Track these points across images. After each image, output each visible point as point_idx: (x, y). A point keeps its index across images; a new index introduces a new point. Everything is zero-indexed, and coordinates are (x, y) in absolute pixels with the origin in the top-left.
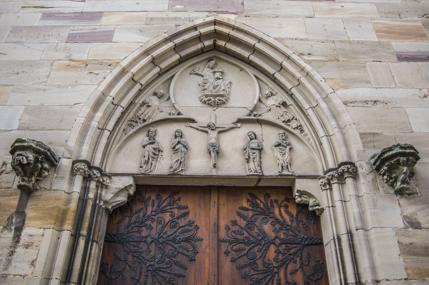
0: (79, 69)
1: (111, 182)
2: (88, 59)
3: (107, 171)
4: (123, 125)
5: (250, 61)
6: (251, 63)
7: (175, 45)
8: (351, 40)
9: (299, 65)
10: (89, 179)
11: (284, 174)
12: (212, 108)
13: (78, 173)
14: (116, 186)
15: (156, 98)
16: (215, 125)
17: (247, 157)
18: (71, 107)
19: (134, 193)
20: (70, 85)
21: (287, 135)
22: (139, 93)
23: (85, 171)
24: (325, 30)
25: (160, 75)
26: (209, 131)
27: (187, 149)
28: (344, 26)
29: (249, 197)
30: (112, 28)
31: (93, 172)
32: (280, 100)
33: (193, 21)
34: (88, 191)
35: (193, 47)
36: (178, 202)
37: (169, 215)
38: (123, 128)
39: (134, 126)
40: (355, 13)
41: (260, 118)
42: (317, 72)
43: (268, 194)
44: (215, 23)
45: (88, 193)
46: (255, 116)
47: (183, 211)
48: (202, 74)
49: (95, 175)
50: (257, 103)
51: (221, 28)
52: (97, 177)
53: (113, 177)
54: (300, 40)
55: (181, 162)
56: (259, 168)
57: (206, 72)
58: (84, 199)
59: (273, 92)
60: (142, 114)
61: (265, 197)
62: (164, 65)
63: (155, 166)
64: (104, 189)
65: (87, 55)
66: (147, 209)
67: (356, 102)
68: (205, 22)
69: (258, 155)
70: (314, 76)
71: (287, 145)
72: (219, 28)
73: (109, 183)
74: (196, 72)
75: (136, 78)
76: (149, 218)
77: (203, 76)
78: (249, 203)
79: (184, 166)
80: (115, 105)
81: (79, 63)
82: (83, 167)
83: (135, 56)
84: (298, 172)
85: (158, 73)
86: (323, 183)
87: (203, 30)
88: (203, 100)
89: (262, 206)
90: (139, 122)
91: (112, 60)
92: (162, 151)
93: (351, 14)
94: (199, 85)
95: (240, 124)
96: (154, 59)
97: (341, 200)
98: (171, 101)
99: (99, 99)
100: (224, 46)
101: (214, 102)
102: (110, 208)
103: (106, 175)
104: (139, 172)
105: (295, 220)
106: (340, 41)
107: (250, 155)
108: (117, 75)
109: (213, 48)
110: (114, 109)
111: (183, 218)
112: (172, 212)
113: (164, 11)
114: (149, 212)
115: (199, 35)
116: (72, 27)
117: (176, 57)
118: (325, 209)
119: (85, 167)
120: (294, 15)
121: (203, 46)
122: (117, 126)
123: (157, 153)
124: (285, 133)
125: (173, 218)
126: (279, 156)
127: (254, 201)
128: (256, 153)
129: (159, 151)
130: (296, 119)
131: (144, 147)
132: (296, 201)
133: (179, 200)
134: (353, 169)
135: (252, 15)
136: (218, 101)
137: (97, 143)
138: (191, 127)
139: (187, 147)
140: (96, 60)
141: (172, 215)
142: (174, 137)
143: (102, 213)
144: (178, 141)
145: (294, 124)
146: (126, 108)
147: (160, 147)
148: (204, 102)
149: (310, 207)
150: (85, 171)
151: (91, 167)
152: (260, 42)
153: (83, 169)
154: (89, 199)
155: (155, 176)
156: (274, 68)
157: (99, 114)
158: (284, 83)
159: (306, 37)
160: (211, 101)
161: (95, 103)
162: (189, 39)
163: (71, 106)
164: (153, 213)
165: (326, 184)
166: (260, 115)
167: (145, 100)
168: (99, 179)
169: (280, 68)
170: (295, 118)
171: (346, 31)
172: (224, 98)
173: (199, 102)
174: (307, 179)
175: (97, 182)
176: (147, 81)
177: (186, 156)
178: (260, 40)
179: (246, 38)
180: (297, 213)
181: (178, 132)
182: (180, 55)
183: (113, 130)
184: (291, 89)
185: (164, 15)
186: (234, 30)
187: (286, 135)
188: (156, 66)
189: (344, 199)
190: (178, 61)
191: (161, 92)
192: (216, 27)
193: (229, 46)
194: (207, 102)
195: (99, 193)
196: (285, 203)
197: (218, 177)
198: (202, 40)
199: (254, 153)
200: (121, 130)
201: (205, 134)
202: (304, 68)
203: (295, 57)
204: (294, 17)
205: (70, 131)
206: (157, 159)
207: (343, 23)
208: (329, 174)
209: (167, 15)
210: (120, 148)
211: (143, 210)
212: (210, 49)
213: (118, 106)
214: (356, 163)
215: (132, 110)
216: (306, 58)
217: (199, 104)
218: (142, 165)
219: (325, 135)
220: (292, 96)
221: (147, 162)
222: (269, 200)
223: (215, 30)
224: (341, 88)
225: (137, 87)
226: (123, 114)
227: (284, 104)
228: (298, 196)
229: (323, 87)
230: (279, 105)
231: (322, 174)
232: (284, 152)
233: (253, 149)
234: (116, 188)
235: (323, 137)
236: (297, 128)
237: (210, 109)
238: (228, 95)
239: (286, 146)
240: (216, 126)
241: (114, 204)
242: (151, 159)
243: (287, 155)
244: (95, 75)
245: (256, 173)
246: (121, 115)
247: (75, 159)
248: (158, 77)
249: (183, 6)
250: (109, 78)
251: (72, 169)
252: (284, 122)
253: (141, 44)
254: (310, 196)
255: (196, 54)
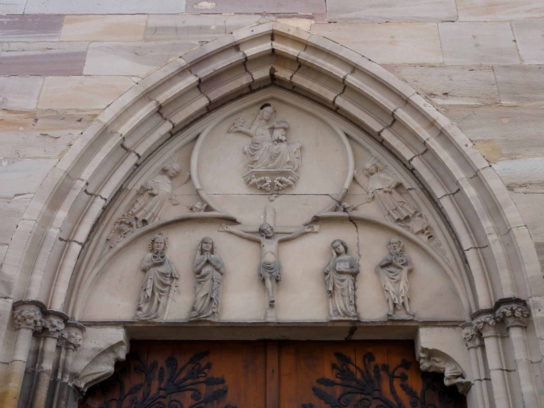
0: (21, 128)
1: (84, 338)
2: (39, 107)
3: (78, 317)
4: (106, 231)
5: (338, 108)
6: (339, 111)
7: (200, 81)
8: (526, 63)
9: (425, 115)
10: (44, 334)
11: (396, 318)
12: (267, 196)
13: (23, 325)
14: (93, 345)
15: (166, 178)
16: (272, 230)
17: (331, 289)
18: (9, 201)
19: (127, 356)
20: (5, 158)
21: (403, 246)
22: (135, 170)
23: (35, 322)
24: (477, 45)
25: (173, 134)
26: (263, 240)
27: (222, 274)
28: (514, 37)
29: (334, 360)
30: (82, 48)
31: (51, 321)
32: (392, 181)
33: (232, 33)
34: (42, 358)
35: (232, 83)
36: (206, 371)
37: (190, 396)
38: (105, 236)
39: (126, 233)
40: (536, 9)
41: (355, 214)
42: (460, 128)
43: (371, 354)
44: (273, 35)
45: (41, 362)
46: (345, 210)
47: (215, 388)
48: (251, 131)
49: (54, 326)
50: (351, 186)
51: (283, 46)
52: (58, 331)
53: (88, 329)
54: (430, 67)
55: (211, 299)
56: (352, 308)
57: (258, 127)
58: (34, 371)
59: (379, 165)
60: (141, 209)
61: (364, 361)
62: (179, 118)
63: (165, 307)
64: (71, 351)
65: (36, 101)
66: (150, 385)
67: (531, 184)
68: (253, 35)
69: (351, 283)
70: (453, 136)
71: (402, 265)
72: (279, 46)
73: (80, 340)
74: (239, 130)
75: (128, 144)
76: (154, 403)
77: (250, 136)
78: (336, 371)
79: (218, 306)
80: (91, 195)
81: (21, 115)
82: (32, 314)
83: (125, 103)
84: (425, 315)
85: (170, 132)
86: (470, 336)
87: (251, 51)
88: (251, 183)
89: (359, 376)
90: (135, 226)
91: (83, 111)
92: (177, 279)
93: (529, 11)
94: (245, 153)
95: (319, 226)
96: (160, 107)
97: (500, 369)
98: (193, 185)
99: (61, 185)
100: (289, 79)
101: (272, 184)
102: (82, 386)
103: (75, 326)
104: (136, 318)
105: (419, 403)
106: (504, 67)
107: (336, 285)
108: (92, 139)
109: (270, 82)
110: (88, 202)
111: (215, 402)
112: (195, 390)
113: (178, 14)
114: (154, 390)
115: (244, 60)
116: (6, 45)
117: (202, 102)
118: (473, 384)
119: (35, 314)
120: (420, 18)
121: (251, 80)
122: (95, 234)
123: (168, 282)
124: (400, 242)
125: (197, 402)
126: (389, 285)
127: (345, 367)
128: (346, 282)
129: (172, 278)
130: (420, 216)
131: (145, 271)
132: (421, 367)
133: (209, 366)
134: (522, 312)
135: (341, 19)
136: (278, 183)
137: (57, 268)
138: (231, 233)
139: (222, 270)
140: (53, 111)
141: (196, 396)
142: (199, 253)
143: (68, 396)
144: (206, 259)
145: (416, 225)
146: (112, 200)
147: (175, 271)
148: (254, 186)
149: (447, 379)
150: (35, 322)
151: (45, 312)
152: (356, 71)
153: (31, 318)
154: (43, 372)
155: (164, 325)
156: (380, 122)
157: (62, 214)
158: (399, 149)
159: (441, 60)
160: (265, 184)
161: (54, 193)
162: (225, 68)
163: (9, 199)
164: (162, 393)
165: (474, 337)
166: (354, 209)
167: (146, 183)
168: (63, 334)
169: (392, 120)
170: (418, 214)
171: (517, 46)
172: (290, 177)
173: (244, 186)
174: (441, 328)
175: (58, 340)
176: (149, 149)
177: (221, 288)
178: (355, 69)
179: (329, 65)
180: (422, 391)
181: (207, 243)
182: (208, 99)
183: (87, 240)
184: (411, 160)
185: (178, 22)
186: (308, 49)
187: (401, 245)
188: (166, 119)
189: (506, 365)
190: (206, 109)
191: (175, 167)
192: (274, 43)
193: (301, 80)
194: (259, 186)
195: (61, 360)
196: (401, 370)
197: (278, 325)
198: (249, 68)
199: (343, 281)
200: (103, 240)
201: (253, 247)
202: (435, 121)
203: (419, 101)
204: (418, 22)
205: (7, 246)
206: (169, 292)
207: (512, 30)
208: (478, 320)
209: (184, 22)
210: (101, 274)
211: (142, 388)
212: (264, 84)
213: (96, 196)
214: (528, 300)
215: (121, 203)
216: (439, 101)
217: (242, 189)
218: (141, 306)
219: (473, 246)
220: (414, 171)
221: (149, 300)
222: (373, 364)
223: (273, 50)
224: (503, 158)
225: (132, 160)
226: (105, 209)
227: (399, 186)
228: (424, 358)
229: (468, 157)
230: (390, 190)
231: (467, 319)
232: (397, 278)
233: (341, 273)
234: (94, 349)
235: (468, 250)
236: (422, 232)
237: (263, 200)
238: (296, 171)
239: (402, 266)
240: (276, 230)
241: (90, 379)
242: (157, 294)
243: (402, 283)
244: (52, 140)
245: (347, 318)
246: (102, 213)
247: (16, 299)
248: (169, 139)
249: (213, 4)
250: (79, 146)
251: (13, 317)
252: (398, 220)
253: (137, 80)
254: (447, 358)
255: (239, 94)
